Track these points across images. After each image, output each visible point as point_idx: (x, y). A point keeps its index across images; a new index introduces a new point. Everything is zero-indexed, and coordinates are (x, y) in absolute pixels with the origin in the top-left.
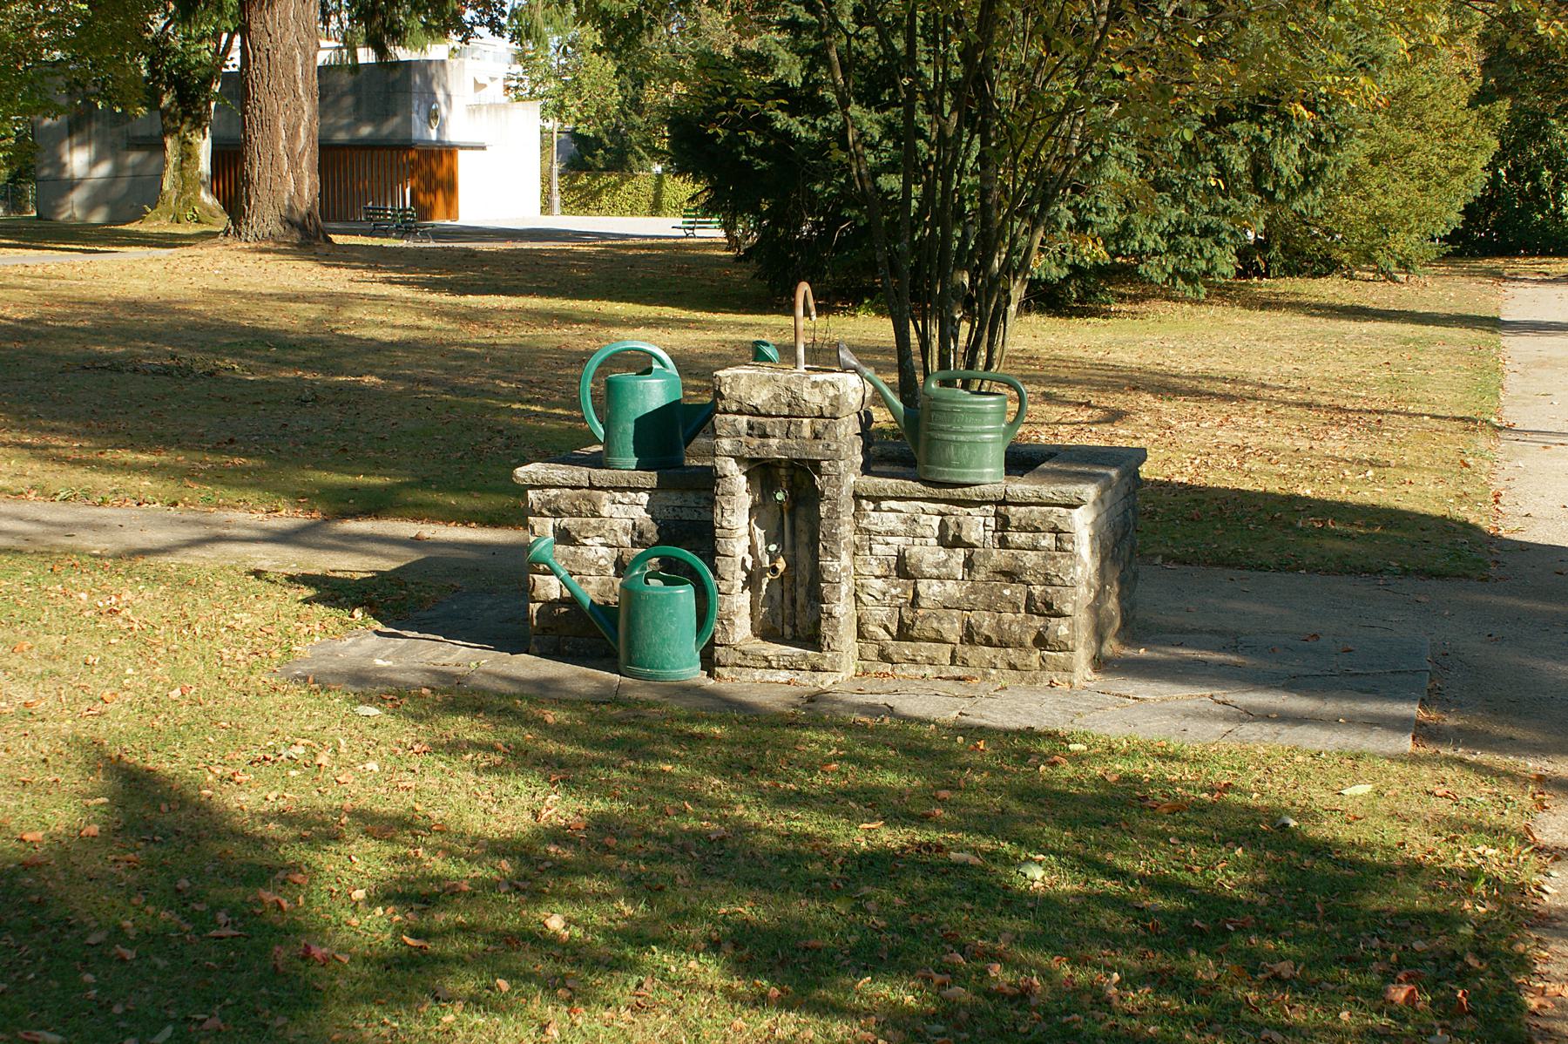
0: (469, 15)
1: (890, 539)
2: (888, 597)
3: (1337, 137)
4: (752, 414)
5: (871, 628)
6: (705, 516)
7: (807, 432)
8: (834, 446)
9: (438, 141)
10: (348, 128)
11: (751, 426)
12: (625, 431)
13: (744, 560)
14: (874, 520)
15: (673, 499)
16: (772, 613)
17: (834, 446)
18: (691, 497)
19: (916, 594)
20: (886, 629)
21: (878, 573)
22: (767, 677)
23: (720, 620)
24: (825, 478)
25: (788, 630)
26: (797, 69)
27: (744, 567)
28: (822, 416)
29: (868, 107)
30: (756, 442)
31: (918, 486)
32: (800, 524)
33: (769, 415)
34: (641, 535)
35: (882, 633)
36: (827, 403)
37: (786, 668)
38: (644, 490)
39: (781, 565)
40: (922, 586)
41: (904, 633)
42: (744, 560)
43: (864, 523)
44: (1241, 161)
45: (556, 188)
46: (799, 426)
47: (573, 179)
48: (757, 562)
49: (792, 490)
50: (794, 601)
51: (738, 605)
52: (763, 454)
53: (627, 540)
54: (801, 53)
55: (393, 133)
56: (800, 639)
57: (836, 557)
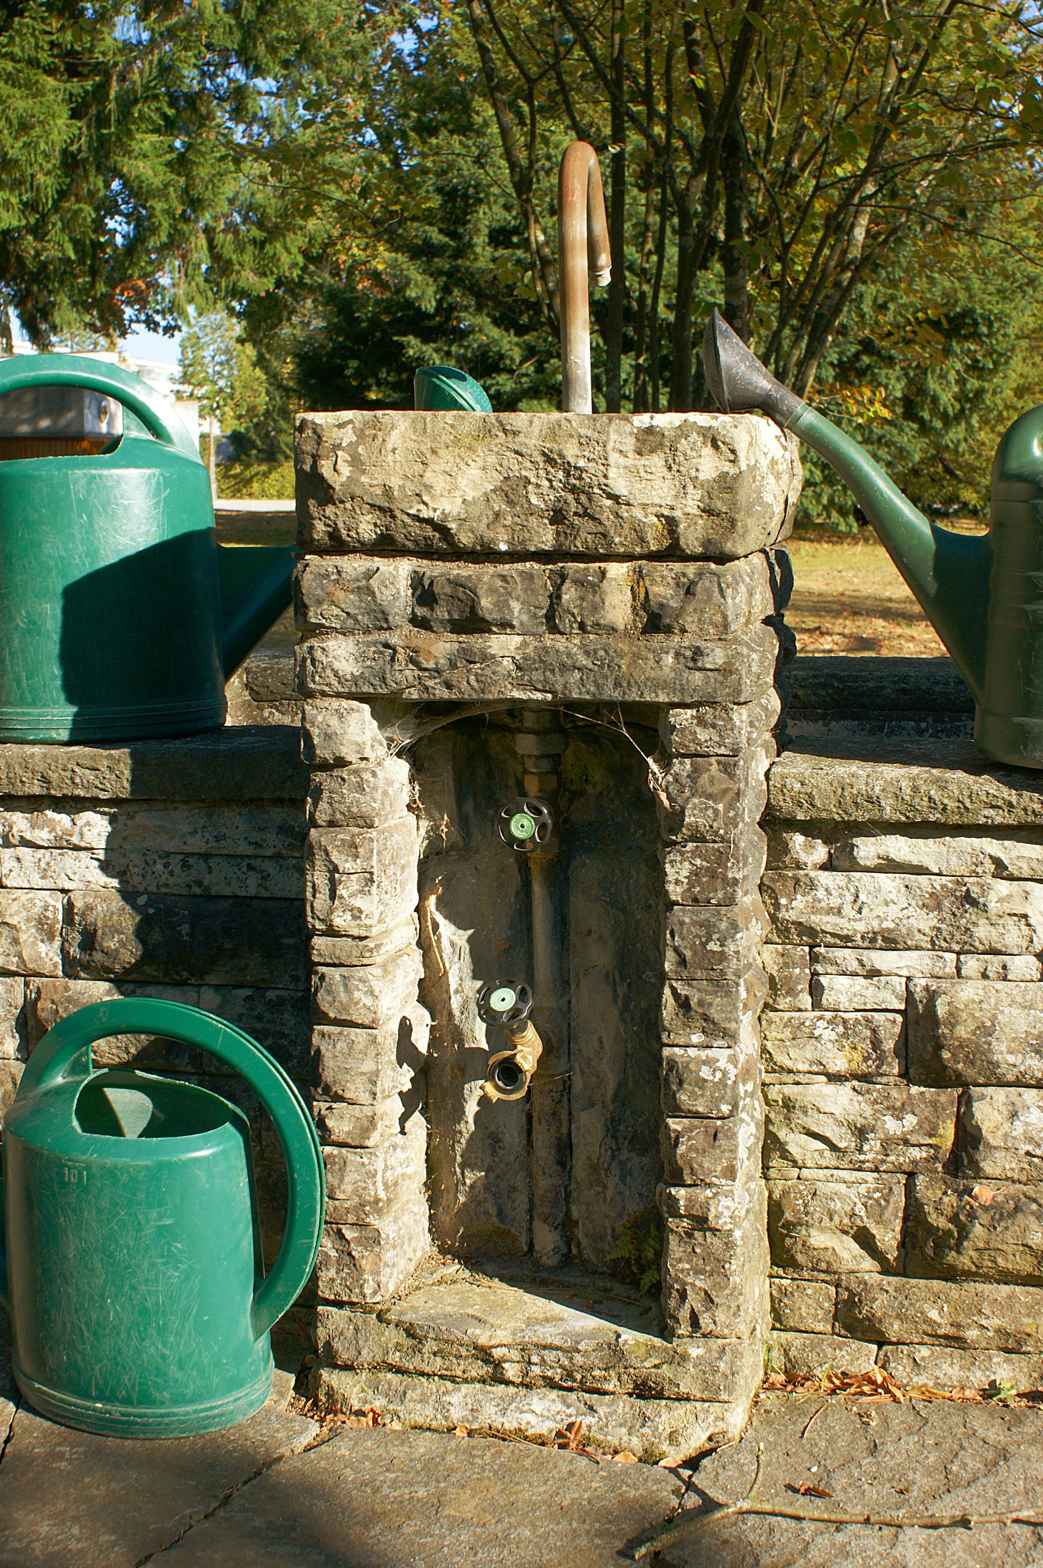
0: (129, 312)
1: (882, 960)
2: (872, 1148)
3: (995, 363)
4: (427, 552)
5: (818, 1239)
6: (280, 885)
7: (618, 607)
8: (717, 657)
9: (108, 433)
10: (29, 421)
11: (424, 592)
12: (34, 627)
13: (405, 1028)
14: (829, 897)
15: (182, 830)
16: (493, 1187)
17: (717, 657)
18: (236, 827)
19: (969, 1137)
20: (864, 1239)
21: (839, 1064)
22: (490, 1415)
23: (335, 1228)
24: (682, 767)
25: (547, 1239)
26: (431, 290)
27: (406, 1052)
28: (673, 552)
29: (507, 330)
30: (442, 646)
31: (988, 786)
32: (588, 911)
33: (485, 554)
34: (89, 940)
35: (848, 1253)
36: (692, 503)
37: (551, 1384)
38: (93, 804)
39: (528, 1051)
40: (990, 1110)
41: (924, 1250)
42: (405, 1028)
43: (796, 908)
44: (899, 386)
45: (213, 476)
46: (593, 587)
47: (228, 468)
48: (445, 1031)
49: (566, 809)
50: (564, 1149)
51: (388, 1168)
52: (466, 687)
53: (48, 954)
54: (435, 275)
55: (69, 424)
56: (587, 1268)
57: (719, 1032)
